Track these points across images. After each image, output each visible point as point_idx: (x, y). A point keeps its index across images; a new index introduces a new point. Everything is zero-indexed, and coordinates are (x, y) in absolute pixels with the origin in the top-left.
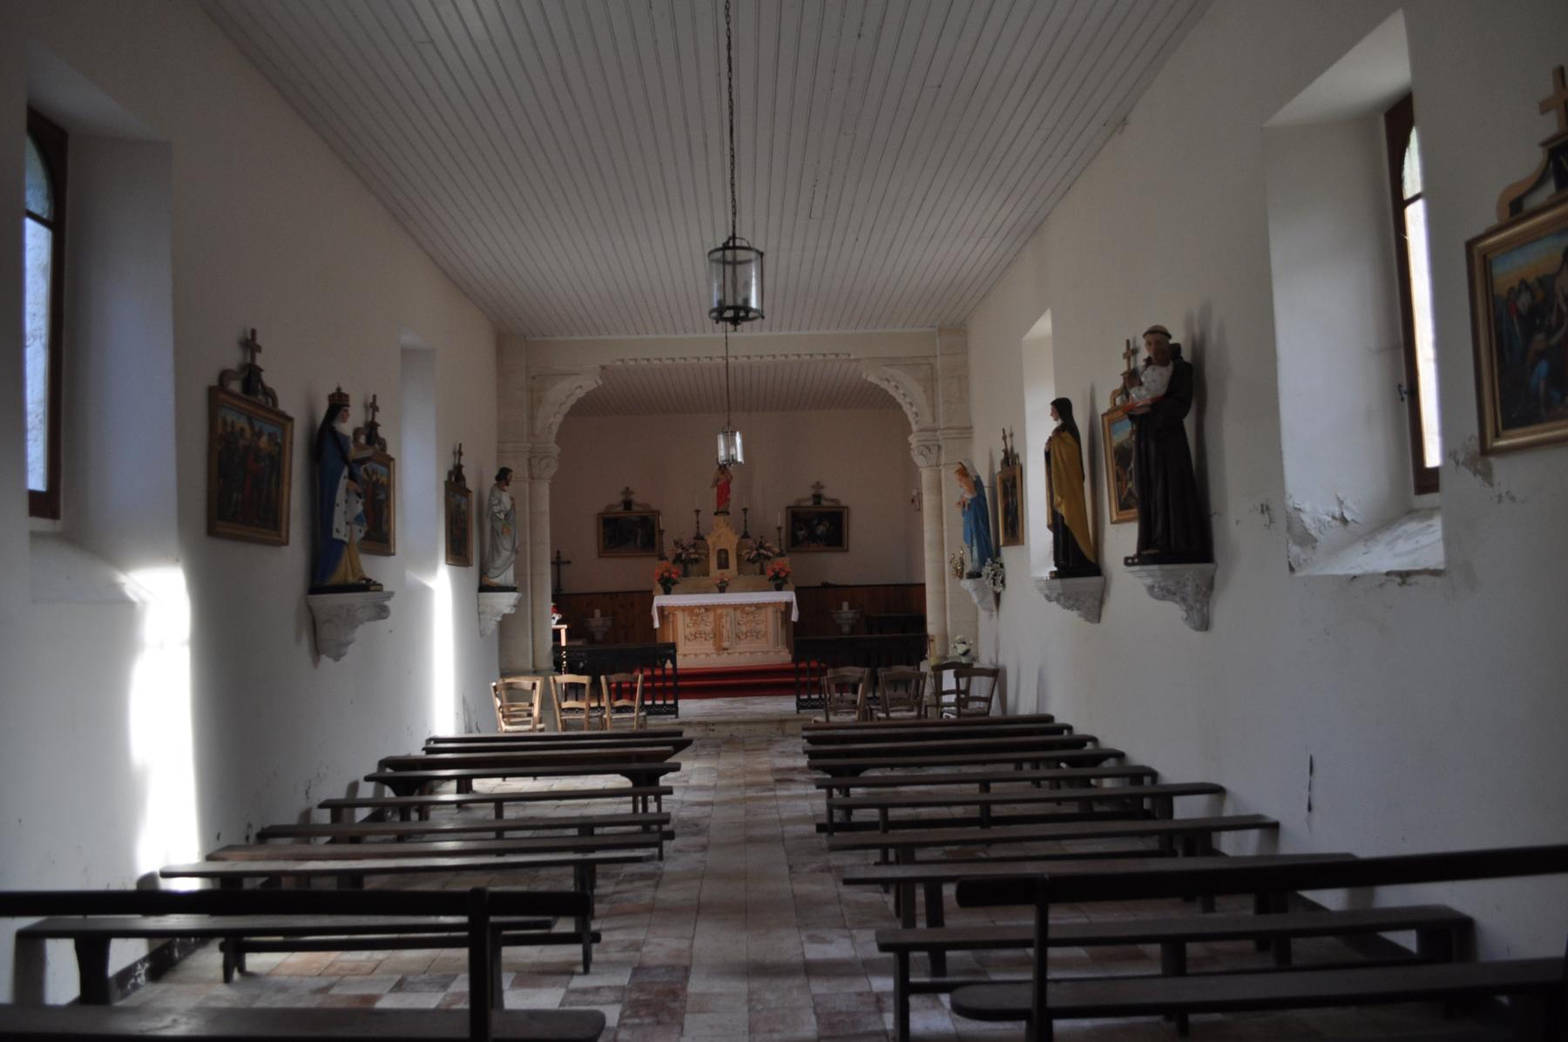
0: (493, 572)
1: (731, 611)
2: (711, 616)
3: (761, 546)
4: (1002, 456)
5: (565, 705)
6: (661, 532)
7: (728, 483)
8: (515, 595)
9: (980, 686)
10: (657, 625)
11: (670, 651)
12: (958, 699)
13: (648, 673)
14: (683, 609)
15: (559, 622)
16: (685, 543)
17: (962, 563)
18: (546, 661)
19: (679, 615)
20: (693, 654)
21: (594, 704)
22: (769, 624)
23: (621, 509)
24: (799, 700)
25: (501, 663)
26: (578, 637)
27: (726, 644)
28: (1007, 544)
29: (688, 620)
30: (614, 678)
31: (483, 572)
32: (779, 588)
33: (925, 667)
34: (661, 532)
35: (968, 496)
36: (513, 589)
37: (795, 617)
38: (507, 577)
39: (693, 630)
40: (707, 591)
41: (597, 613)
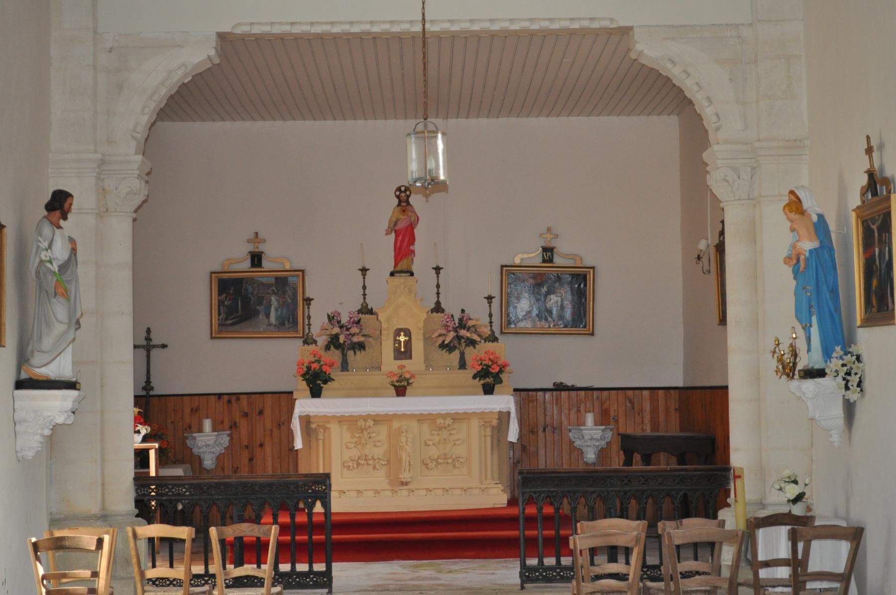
0: (36, 360)
1: (414, 424)
2: (382, 432)
3: (462, 324)
4: (864, 180)
5: (151, 574)
6: (308, 301)
7: (411, 227)
8: (73, 393)
9: (827, 556)
10: (298, 444)
11: (319, 486)
12: (795, 574)
13: (284, 519)
14: (341, 420)
15: (145, 439)
16: (344, 320)
17: (795, 355)
18: (123, 498)
19: (334, 428)
20: (354, 494)
21: (198, 569)
22: (474, 444)
23: (246, 265)
24: (523, 566)
25: (701, 543)
26: (176, 462)
27: (405, 476)
28: (868, 322)
29: (347, 437)
30: (232, 531)
31: (23, 359)
32: (488, 390)
33: (732, 518)
34: (308, 301)
35: (808, 245)
36: (71, 385)
37: (513, 435)
38: (60, 367)
39: (355, 453)
40: (376, 392)
41: (207, 424)
